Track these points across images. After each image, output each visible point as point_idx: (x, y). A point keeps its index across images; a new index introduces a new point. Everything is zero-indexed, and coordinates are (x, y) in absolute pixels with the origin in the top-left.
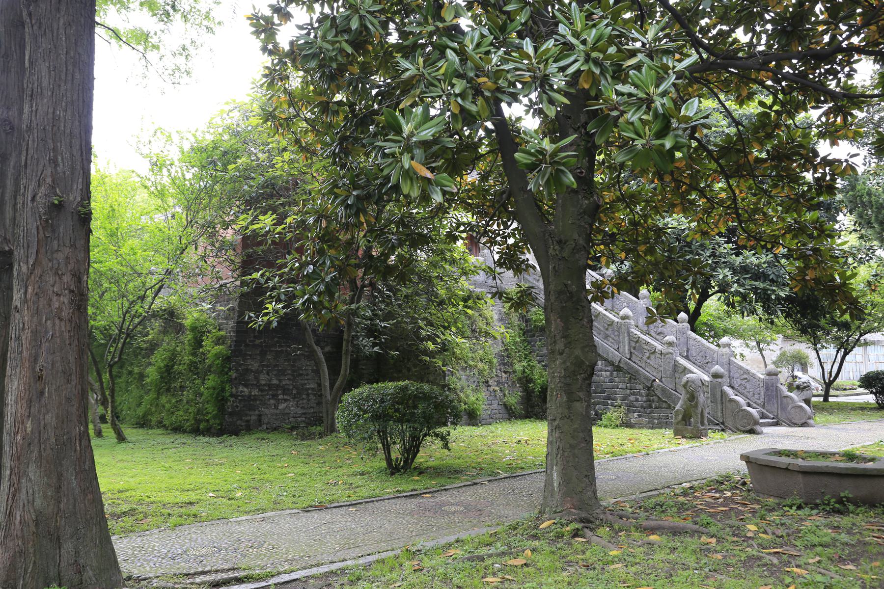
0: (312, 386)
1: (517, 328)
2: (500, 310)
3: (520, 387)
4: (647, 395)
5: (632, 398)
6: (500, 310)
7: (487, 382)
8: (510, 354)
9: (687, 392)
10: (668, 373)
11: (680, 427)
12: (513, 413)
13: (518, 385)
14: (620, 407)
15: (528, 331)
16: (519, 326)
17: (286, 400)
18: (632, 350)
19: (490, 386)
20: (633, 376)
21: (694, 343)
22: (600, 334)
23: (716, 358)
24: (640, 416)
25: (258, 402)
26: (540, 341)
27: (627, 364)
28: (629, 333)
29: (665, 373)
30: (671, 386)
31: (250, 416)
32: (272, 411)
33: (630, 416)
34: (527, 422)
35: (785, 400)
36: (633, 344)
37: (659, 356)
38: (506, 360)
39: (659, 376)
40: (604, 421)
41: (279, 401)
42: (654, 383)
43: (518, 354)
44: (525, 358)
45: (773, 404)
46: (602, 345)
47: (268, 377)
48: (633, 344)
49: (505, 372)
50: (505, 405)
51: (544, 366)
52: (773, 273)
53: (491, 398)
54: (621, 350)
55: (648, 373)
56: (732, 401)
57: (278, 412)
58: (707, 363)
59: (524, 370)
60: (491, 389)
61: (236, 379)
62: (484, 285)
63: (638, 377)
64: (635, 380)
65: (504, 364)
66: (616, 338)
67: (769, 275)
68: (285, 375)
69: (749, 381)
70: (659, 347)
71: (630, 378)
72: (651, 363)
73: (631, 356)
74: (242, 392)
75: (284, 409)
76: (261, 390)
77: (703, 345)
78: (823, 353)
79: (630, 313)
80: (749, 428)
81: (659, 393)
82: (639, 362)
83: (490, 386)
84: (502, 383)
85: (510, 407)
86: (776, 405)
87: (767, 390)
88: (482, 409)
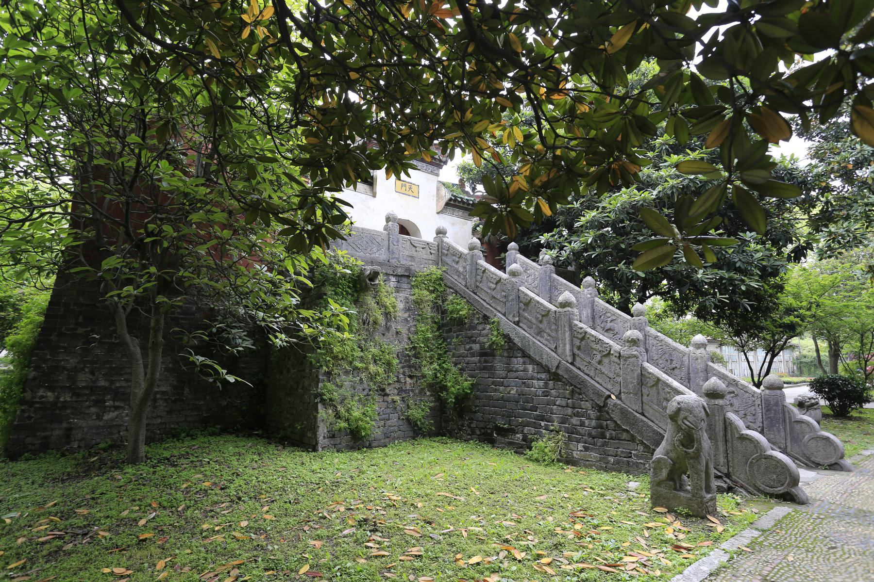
0: (164, 389)
1: (430, 321)
2: (407, 298)
3: (431, 395)
4: (598, 419)
5: (575, 421)
6: (407, 298)
7: (383, 390)
8: (419, 353)
9: (679, 429)
10: (631, 386)
11: (663, 490)
12: (420, 429)
13: (428, 393)
14: (558, 432)
15: (443, 325)
16: (432, 318)
17: (116, 408)
18: (576, 351)
19: (388, 395)
20: (577, 389)
21: (655, 342)
22: (531, 328)
23: (686, 363)
24: (586, 449)
25: (68, 411)
26: (457, 338)
27: (568, 370)
28: (571, 326)
29: (626, 387)
30: (636, 408)
31: (52, 430)
32: (91, 423)
33: (571, 446)
34: (435, 444)
35: (797, 427)
36: (577, 342)
37: (616, 360)
38: (413, 360)
39: (616, 389)
40: (534, 453)
41: (104, 410)
42: (608, 401)
43: (428, 354)
44: (439, 359)
45: (779, 431)
46: (534, 343)
47: (91, 377)
48: (577, 342)
49: (411, 377)
50: (408, 420)
51: (461, 369)
52: (740, 260)
53: (388, 411)
54: (560, 351)
55: (599, 384)
56: (744, 438)
57: (101, 424)
58: (673, 369)
59: (436, 374)
60: (389, 399)
61: (34, 379)
62: (386, 265)
63: (584, 390)
64: (580, 394)
65: (410, 367)
66: (553, 334)
67: (735, 263)
68: (122, 375)
69: (737, 395)
70: (616, 347)
71: (573, 391)
72: (603, 370)
73: (574, 359)
74: (42, 397)
75: (112, 420)
76: (75, 394)
77: (668, 345)
78: (750, 355)
79: (573, 299)
80: (781, 490)
81: (616, 416)
82: (585, 369)
83: (388, 395)
84: (405, 391)
85: (415, 422)
86: (783, 434)
87: (768, 410)
88: (373, 428)
